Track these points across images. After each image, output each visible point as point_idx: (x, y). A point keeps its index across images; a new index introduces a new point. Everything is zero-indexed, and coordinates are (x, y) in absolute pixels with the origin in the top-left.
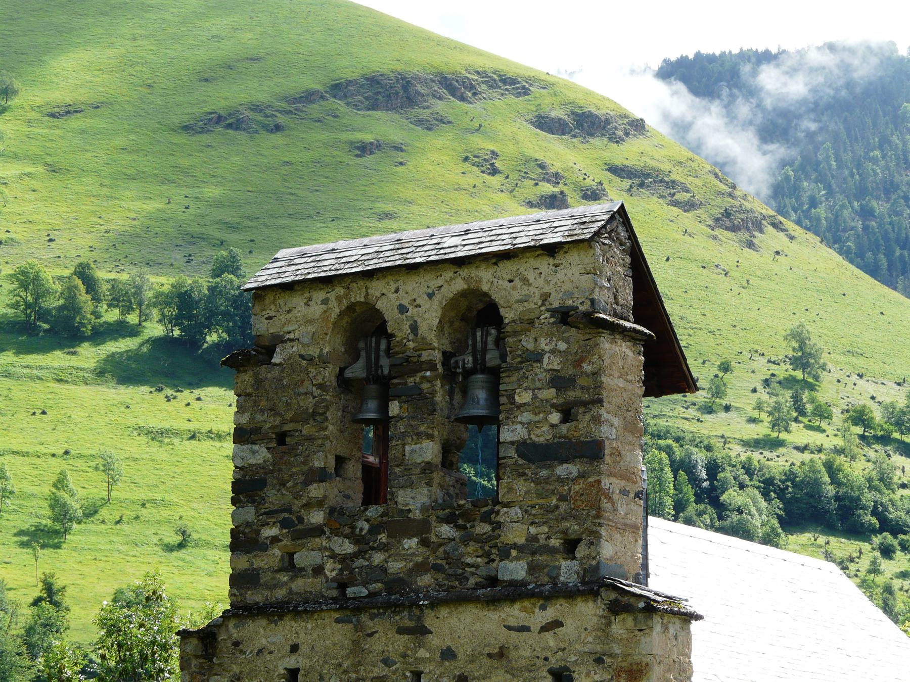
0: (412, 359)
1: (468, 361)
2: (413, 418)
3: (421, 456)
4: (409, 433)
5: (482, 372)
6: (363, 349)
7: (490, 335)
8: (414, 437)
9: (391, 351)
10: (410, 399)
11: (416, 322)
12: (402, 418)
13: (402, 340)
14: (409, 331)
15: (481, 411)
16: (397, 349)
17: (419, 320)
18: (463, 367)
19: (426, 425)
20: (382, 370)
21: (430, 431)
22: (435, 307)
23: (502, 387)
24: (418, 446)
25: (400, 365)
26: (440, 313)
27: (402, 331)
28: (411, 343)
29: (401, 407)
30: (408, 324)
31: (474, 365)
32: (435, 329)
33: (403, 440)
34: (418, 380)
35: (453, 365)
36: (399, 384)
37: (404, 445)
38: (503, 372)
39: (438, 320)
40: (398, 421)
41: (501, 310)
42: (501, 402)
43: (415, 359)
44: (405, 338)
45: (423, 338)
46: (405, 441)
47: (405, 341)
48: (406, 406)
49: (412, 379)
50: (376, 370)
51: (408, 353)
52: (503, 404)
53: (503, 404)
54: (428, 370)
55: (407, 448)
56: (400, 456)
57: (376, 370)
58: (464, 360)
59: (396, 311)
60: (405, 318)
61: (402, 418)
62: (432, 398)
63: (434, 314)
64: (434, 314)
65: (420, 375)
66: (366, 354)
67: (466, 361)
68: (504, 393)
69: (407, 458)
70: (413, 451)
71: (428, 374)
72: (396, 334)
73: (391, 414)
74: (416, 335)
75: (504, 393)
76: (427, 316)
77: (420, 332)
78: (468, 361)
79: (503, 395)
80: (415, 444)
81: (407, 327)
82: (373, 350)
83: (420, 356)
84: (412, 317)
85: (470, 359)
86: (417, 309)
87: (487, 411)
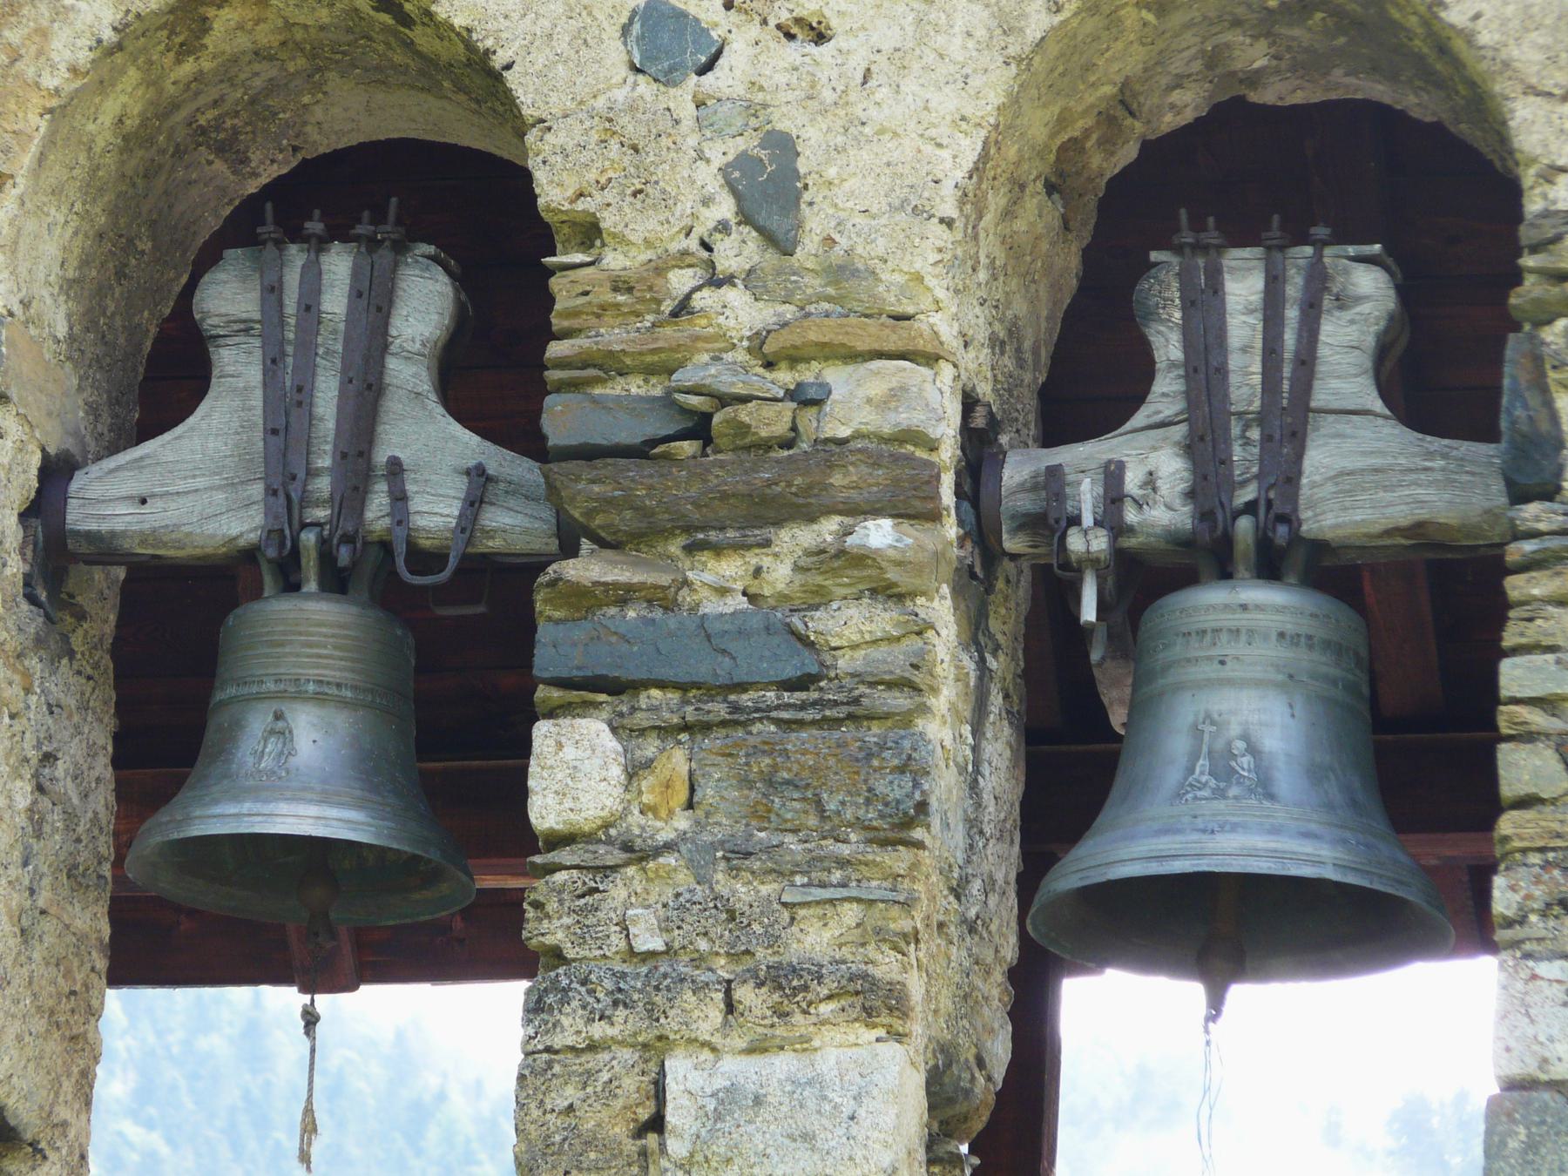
0: (744, 414)
1: (1150, 481)
2: (738, 855)
3: (807, 1137)
4: (698, 960)
5: (1269, 567)
6: (246, 328)
7: (1342, 302)
8: (746, 994)
9: (555, 349)
10: (719, 710)
11: (783, 146)
12: (639, 853)
13: (659, 269)
14: (725, 208)
15: (1260, 842)
16: (614, 336)
17: (813, 140)
18: (1112, 518)
19: (850, 914)
20: (399, 498)
21: (886, 965)
22: (956, 47)
23: (1514, 676)
24: (782, 1064)
25: (640, 452)
26: (995, 97)
27: (667, 201)
28: (735, 296)
29: (635, 771)
30: (721, 152)
31: (1204, 516)
32: (949, 209)
33: (652, 1014)
34: (780, 574)
35: (1026, 503)
36: (623, 595)
37: (655, 1050)
38: (1530, 565)
39: (969, 148)
40: (607, 870)
41: (1101, 195)
42: (1510, 786)
43: (772, 421)
44: (683, 259)
45: (841, 272)
46: (670, 1025)
47: (681, 281)
48: (677, 761)
49: (731, 568)
50: (352, 495)
51: (700, 370)
52: (1526, 802)
53: (1526, 802)
54: (876, 512)
55: (681, 1071)
56: (620, 1131)
57: (352, 495)
58: (1113, 475)
59: (614, 55)
60: (687, 111)
61: (639, 853)
62: (905, 720)
63: (948, 102)
64: (948, 102)
65: (796, 539)
66: (272, 364)
67: (1132, 481)
68: (1537, 719)
69: (677, 1147)
70: (727, 1100)
71: (879, 534)
72: (608, 221)
73: (545, 812)
74: (780, 243)
75: (1537, 719)
76: (883, 107)
77: (815, 223)
78: (1150, 481)
79: (1528, 737)
80: (754, 1049)
81: (708, 177)
82: (331, 341)
83: (807, 399)
84: (752, 109)
85: (1171, 467)
86: (792, 53)
87: (1339, 854)
